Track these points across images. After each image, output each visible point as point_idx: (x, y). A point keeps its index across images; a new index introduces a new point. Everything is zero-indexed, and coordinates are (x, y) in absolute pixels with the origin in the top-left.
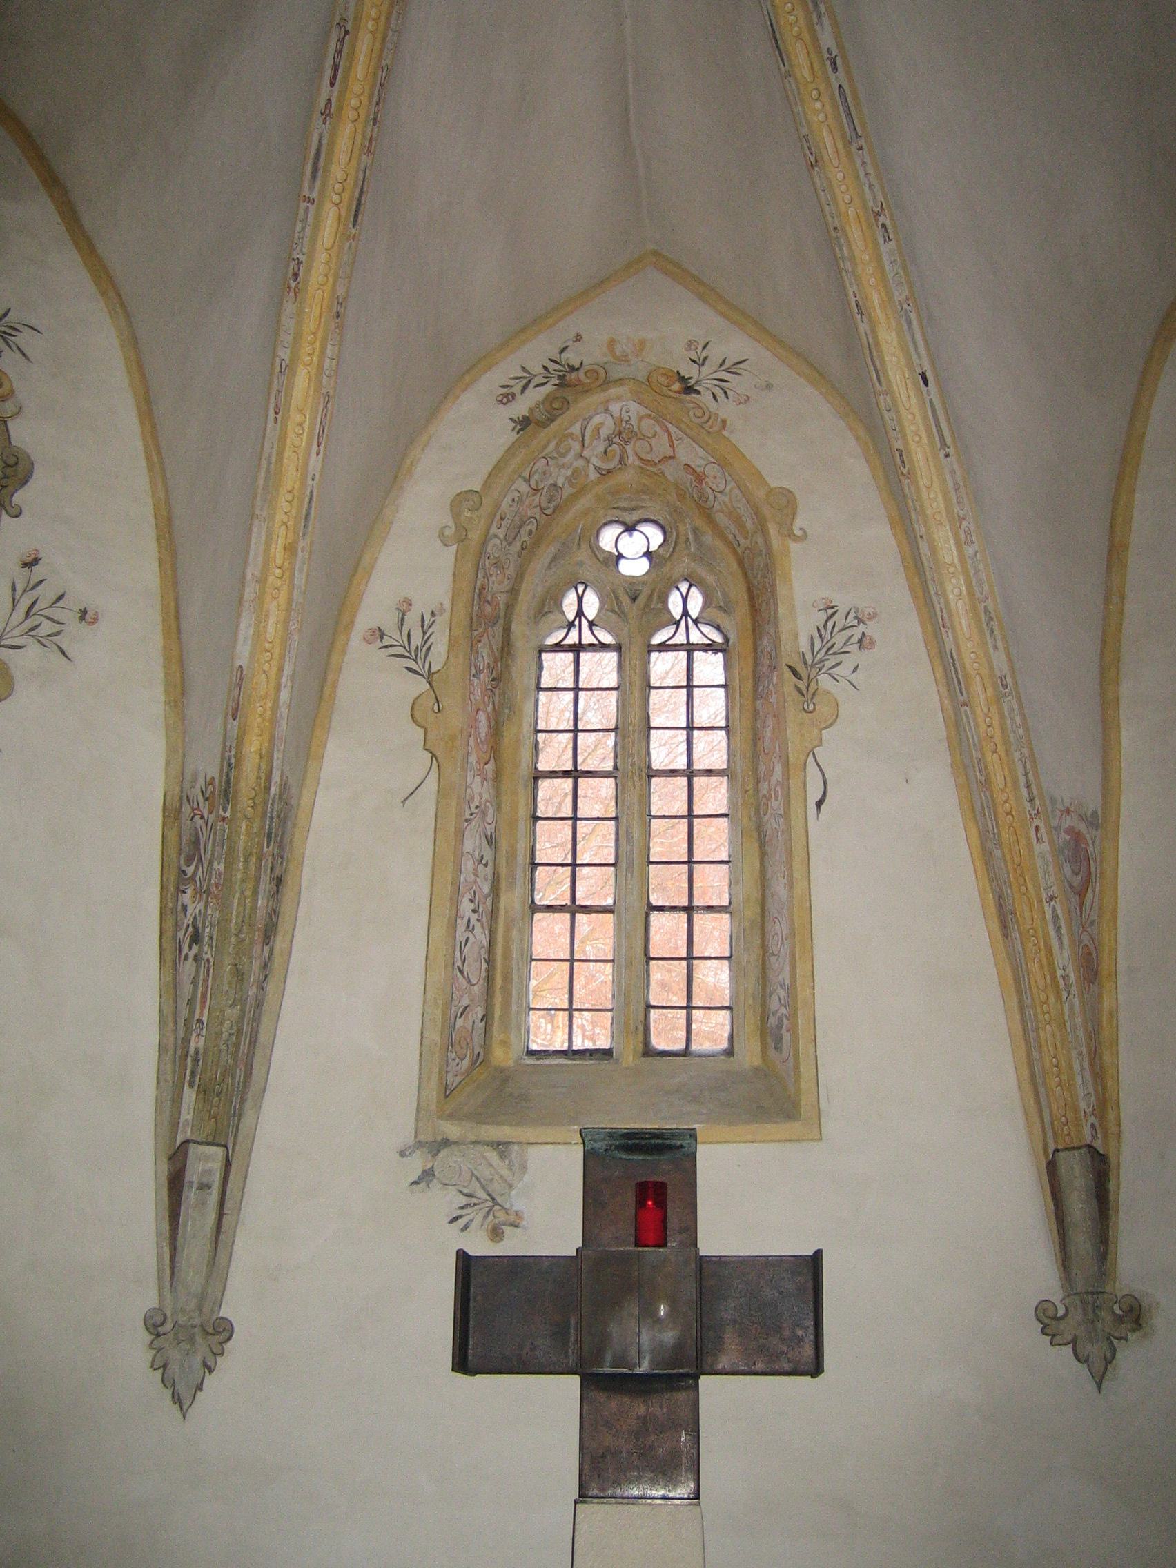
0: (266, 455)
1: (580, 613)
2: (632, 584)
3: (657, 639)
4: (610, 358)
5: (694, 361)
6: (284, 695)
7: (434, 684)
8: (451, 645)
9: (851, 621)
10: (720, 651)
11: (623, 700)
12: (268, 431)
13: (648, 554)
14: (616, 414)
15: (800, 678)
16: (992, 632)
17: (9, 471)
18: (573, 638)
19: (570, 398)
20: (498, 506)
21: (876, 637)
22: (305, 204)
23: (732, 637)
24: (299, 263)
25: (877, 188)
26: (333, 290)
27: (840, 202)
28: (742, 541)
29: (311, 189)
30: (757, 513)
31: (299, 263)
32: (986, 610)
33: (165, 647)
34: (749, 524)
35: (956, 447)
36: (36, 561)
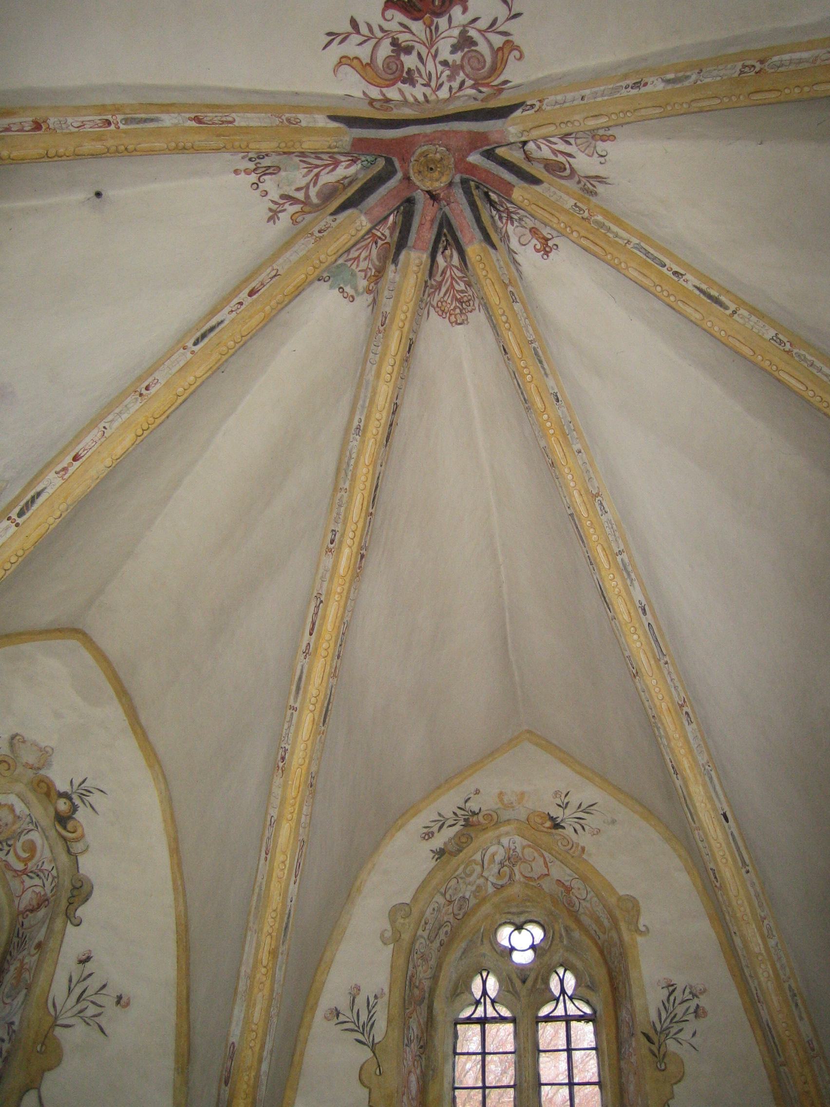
0: (258, 884)
1: (485, 993)
2: (522, 970)
3: (545, 1011)
4: (500, 805)
5: (559, 806)
6: (265, 1067)
7: (376, 1052)
8: (389, 1022)
9: (687, 996)
10: (590, 1021)
11: (519, 1062)
12: (260, 866)
13: (533, 947)
14: (506, 845)
15: (653, 1043)
16: (797, 1005)
17: (75, 893)
18: (480, 1012)
19: (473, 836)
20: (423, 913)
21: (707, 1008)
22: (291, 711)
23: (599, 1008)
24: (286, 750)
25: (680, 688)
26: (308, 768)
27: (656, 700)
28: (601, 935)
29: (295, 701)
30: (610, 913)
31: (286, 750)
32: (790, 987)
33: (177, 1024)
34: (606, 923)
35: (753, 866)
36: (88, 959)
